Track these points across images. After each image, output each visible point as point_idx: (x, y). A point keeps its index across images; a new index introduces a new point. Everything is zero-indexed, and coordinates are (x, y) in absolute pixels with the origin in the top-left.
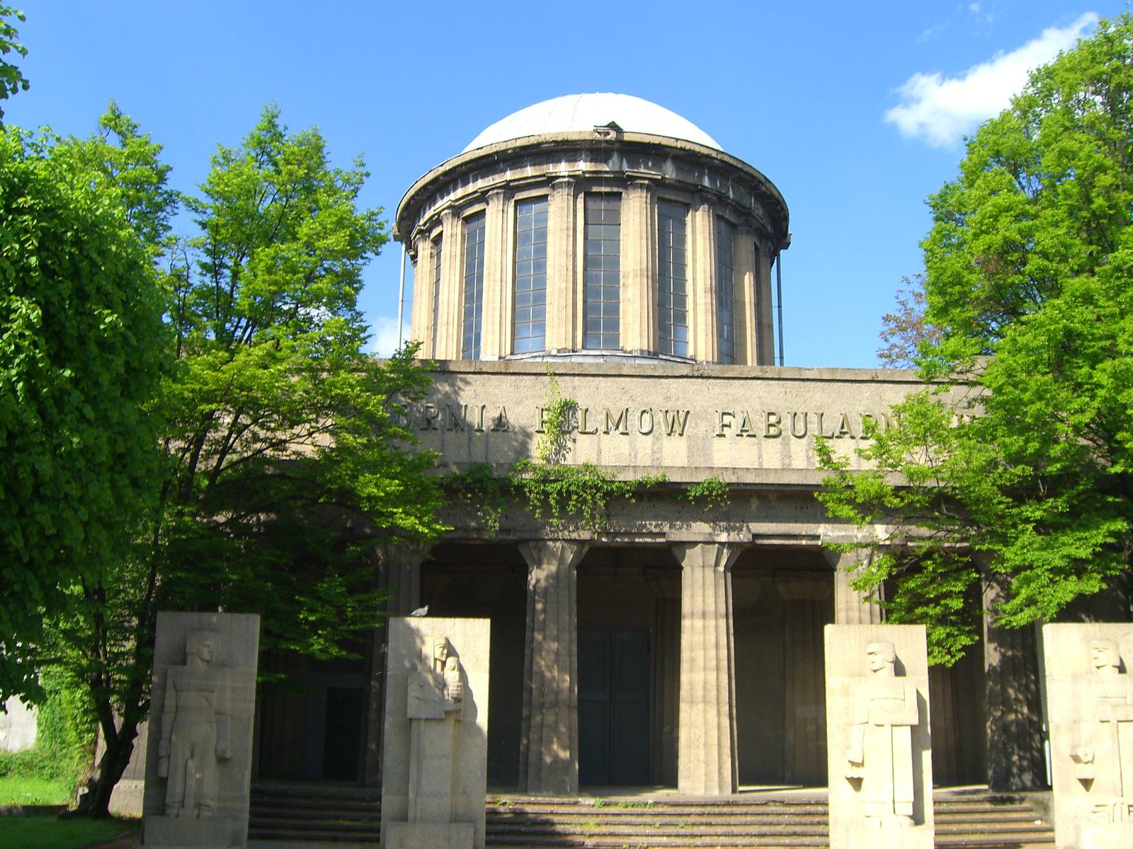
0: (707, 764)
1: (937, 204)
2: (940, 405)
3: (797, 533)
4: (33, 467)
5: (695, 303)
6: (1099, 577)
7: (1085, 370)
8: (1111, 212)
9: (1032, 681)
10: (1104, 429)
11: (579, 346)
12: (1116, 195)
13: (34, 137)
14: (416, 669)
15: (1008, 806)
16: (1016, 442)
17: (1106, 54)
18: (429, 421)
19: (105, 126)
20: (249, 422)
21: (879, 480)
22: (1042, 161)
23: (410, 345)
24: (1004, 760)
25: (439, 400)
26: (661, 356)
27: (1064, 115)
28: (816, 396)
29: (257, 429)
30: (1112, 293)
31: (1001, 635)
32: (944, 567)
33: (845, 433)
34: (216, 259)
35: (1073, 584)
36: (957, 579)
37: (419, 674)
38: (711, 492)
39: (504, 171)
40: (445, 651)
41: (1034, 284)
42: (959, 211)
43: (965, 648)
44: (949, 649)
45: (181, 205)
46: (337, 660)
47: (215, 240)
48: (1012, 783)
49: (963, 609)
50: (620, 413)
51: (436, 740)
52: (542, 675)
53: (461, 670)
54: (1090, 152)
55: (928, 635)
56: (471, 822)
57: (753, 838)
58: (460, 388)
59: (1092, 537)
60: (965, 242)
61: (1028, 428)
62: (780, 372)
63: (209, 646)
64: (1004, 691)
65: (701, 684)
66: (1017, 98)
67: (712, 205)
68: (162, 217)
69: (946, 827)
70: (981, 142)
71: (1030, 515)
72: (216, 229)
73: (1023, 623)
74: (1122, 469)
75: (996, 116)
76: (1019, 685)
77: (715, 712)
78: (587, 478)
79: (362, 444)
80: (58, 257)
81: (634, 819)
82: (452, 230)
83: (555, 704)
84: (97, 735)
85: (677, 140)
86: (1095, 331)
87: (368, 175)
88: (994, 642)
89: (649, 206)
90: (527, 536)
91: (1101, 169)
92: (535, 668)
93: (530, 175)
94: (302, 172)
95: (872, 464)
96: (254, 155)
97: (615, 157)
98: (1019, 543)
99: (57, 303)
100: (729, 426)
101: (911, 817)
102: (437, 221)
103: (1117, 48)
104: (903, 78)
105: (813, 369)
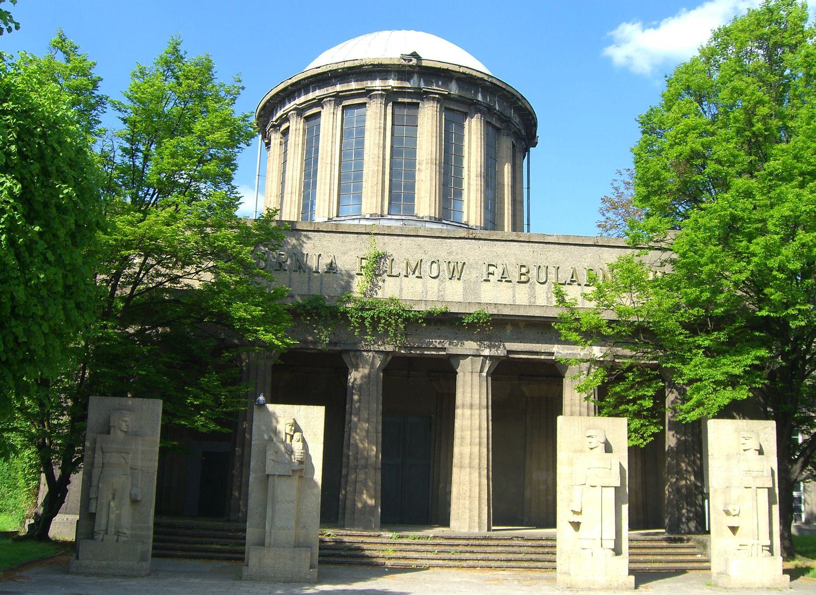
0: (470, 511)
1: (644, 121)
2: (641, 264)
3: (538, 350)
4: (12, 294)
5: (469, 184)
6: (747, 388)
7: (744, 243)
8: (766, 133)
9: (698, 458)
10: (755, 284)
11: (386, 212)
12: (770, 122)
13: (14, 59)
14: (273, 440)
15: (679, 544)
16: (693, 292)
17: (768, 20)
18: (280, 265)
19: (54, 46)
20: (154, 262)
21: (598, 316)
22: (719, 94)
23: (271, 211)
24: (677, 512)
25: (288, 249)
26: (444, 221)
27: (736, 62)
28: (554, 255)
29: (159, 267)
30: (765, 191)
31: (677, 426)
32: (640, 377)
33: (575, 281)
34: (132, 145)
35: (729, 392)
36: (649, 387)
37: (275, 444)
38: (479, 320)
39: (335, 85)
40: (293, 428)
41: (710, 181)
42: (660, 128)
43: (653, 434)
44: (642, 435)
45: (108, 105)
46: (214, 432)
47: (133, 132)
48: (682, 529)
49: (653, 407)
50: (416, 263)
51: (285, 490)
52: (357, 446)
53: (304, 441)
54: (754, 90)
55: (629, 425)
56: (309, 547)
57: (502, 562)
58: (303, 242)
59: (744, 360)
60: (663, 150)
61: (701, 283)
62: (530, 237)
63: (126, 421)
64: (678, 465)
65: (468, 455)
66: (703, 49)
67: (483, 114)
68: (94, 114)
69: (635, 558)
70: (677, 79)
71: (701, 343)
72: (134, 124)
73: (694, 418)
74: (767, 313)
75: (688, 61)
76: (689, 460)
77: (477, 474)
78: (392, 308)
79: (236, 281)
80: (29, 145)
81: (419, 547)
82: (296, 125)
83: (365, 467)
84: (39, 483)
85: (460, 66)
86: (753, 216)
87: (243, 88)
88: (672, 430)
89: (438, 114)
90: (349, 348)
91: (761, 102)
92: (352, 441)
93: (354, 88)
94: (197, 85)
95: (593, 304)
96: (162, 71)
97: (415, 77)
98: (692, 363)
99: (29, 178)
100: (493, 274)
101: (613, 550)
102: (285, 119)
103: (775, 17)
104: (615, 26)
105: (553, 236)
